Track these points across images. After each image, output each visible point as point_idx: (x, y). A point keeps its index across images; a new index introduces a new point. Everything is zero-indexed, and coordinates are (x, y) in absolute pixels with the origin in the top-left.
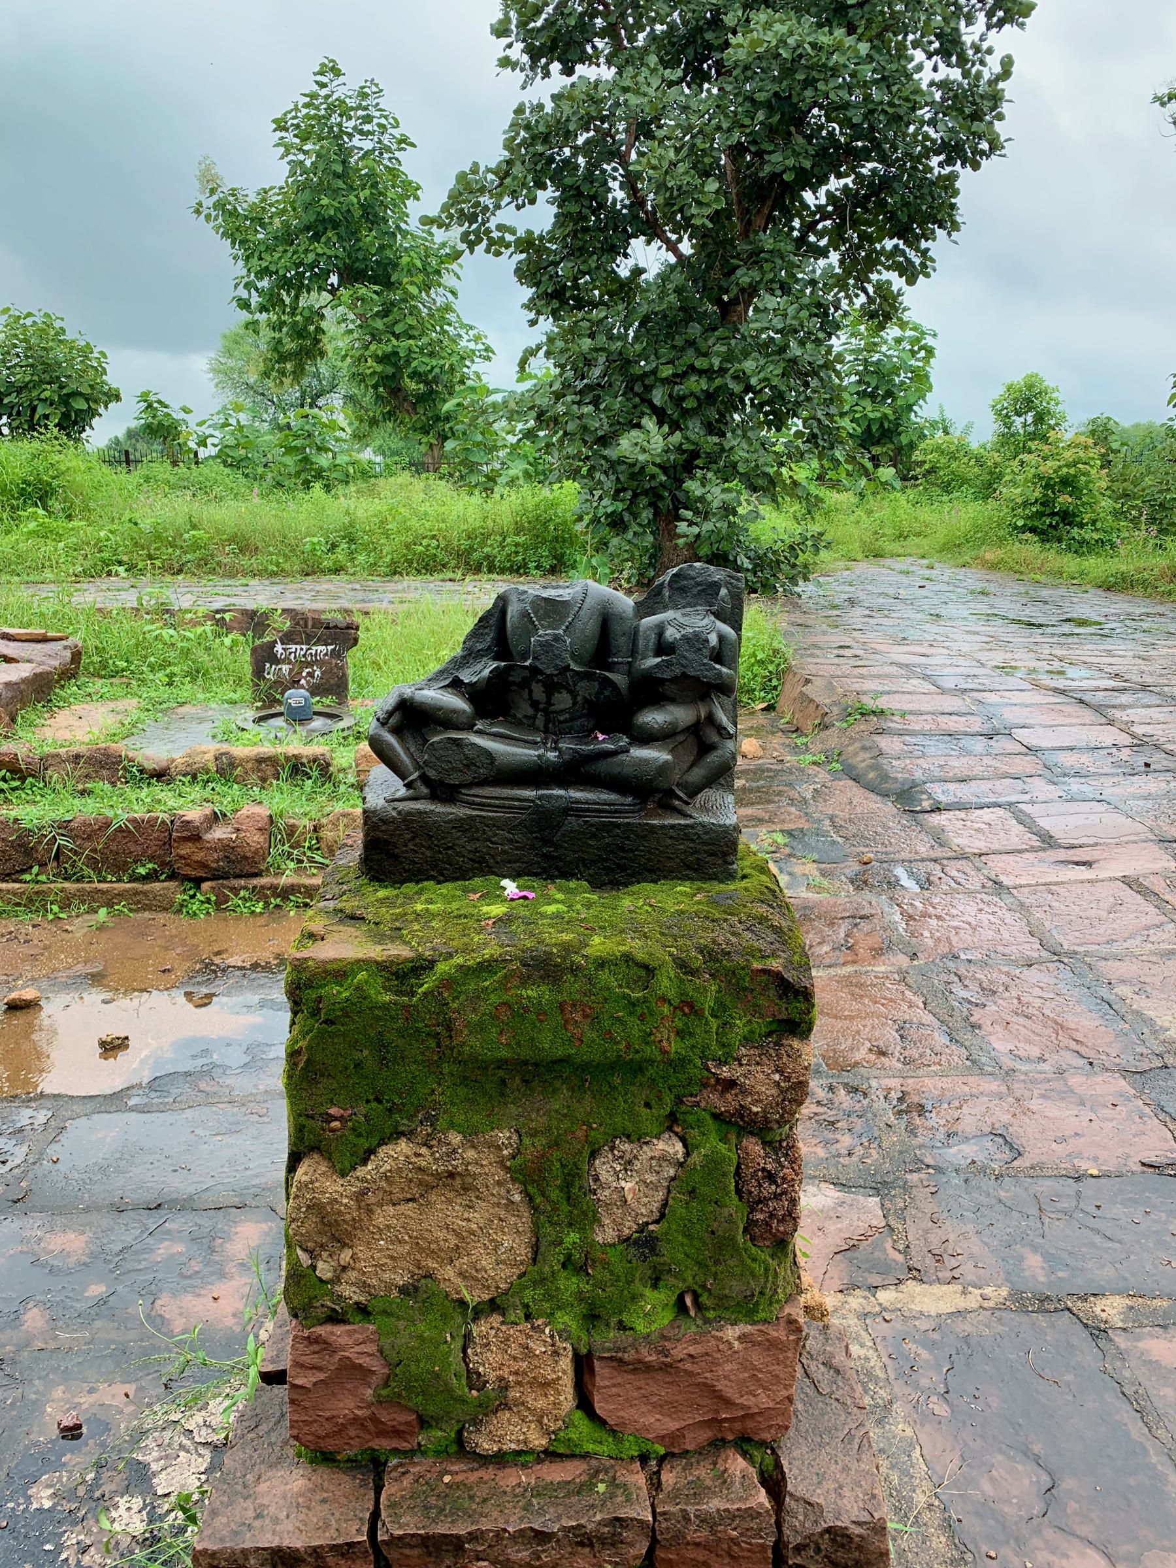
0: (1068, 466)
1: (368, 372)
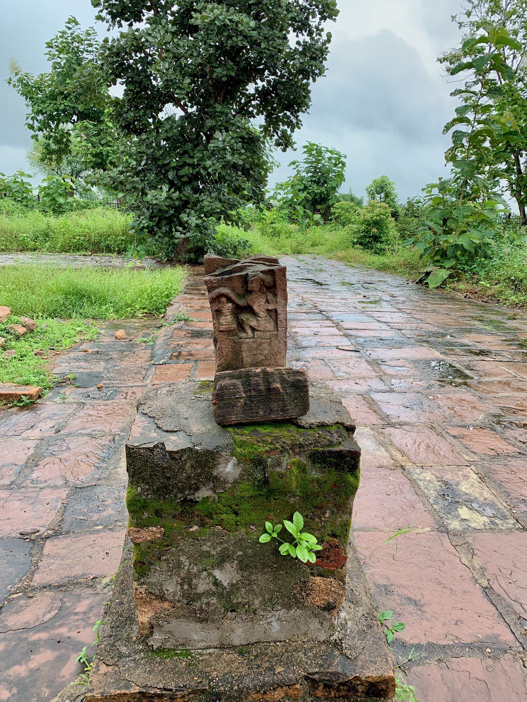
0: (377, 216)
1: (88, 161)
